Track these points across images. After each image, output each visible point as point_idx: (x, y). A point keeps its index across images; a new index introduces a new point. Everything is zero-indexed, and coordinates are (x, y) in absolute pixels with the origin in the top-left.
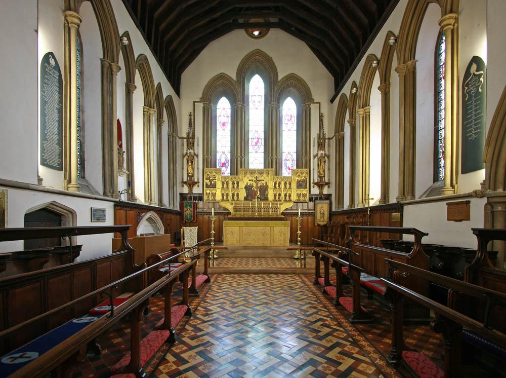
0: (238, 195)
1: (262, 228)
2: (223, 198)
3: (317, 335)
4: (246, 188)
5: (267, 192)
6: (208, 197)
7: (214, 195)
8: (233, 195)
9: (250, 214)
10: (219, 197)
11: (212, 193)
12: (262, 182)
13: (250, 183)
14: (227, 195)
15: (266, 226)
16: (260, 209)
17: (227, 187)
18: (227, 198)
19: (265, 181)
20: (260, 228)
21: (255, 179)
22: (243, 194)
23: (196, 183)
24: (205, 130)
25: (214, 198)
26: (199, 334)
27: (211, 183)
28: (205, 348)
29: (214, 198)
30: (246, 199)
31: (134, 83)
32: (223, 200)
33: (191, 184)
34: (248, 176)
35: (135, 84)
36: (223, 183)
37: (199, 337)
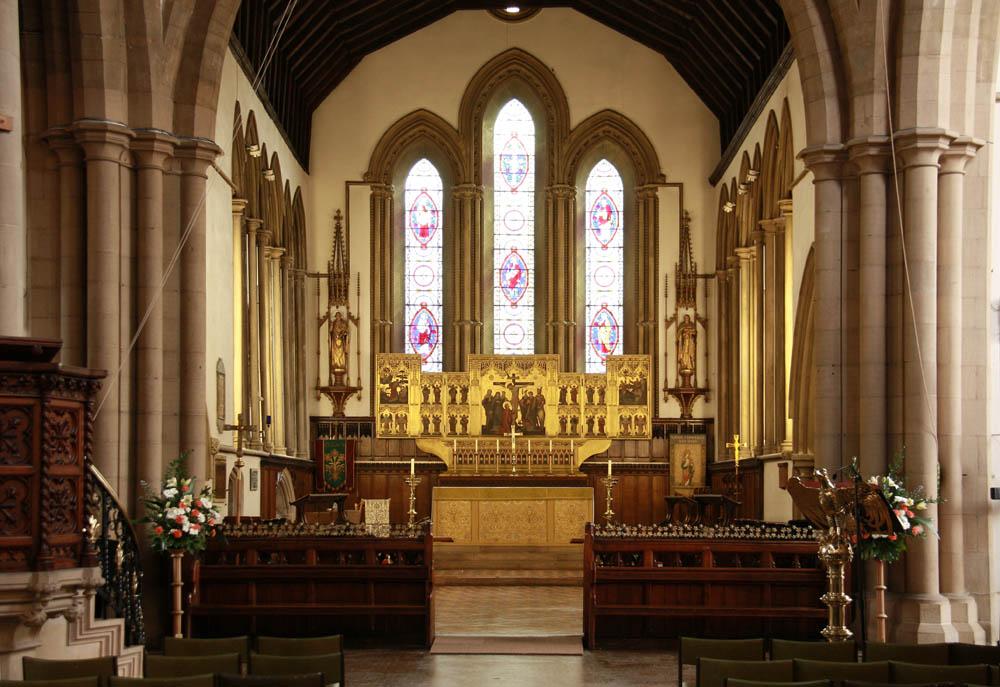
1: (527, 503)
2: (426, 428)
4: (486, 403)
5: (541, 414)
7: (403, 421)
9: (496, 469)
10: (414, 427)
11: (397, 417)
12: (529, 388)
13: (495, 390)
14: (437, 421)
16: (522, 456)
17: (438, 401)
20: (521, 503)
23: (354, 390)
30: (486, 431)
32: (425, 434)
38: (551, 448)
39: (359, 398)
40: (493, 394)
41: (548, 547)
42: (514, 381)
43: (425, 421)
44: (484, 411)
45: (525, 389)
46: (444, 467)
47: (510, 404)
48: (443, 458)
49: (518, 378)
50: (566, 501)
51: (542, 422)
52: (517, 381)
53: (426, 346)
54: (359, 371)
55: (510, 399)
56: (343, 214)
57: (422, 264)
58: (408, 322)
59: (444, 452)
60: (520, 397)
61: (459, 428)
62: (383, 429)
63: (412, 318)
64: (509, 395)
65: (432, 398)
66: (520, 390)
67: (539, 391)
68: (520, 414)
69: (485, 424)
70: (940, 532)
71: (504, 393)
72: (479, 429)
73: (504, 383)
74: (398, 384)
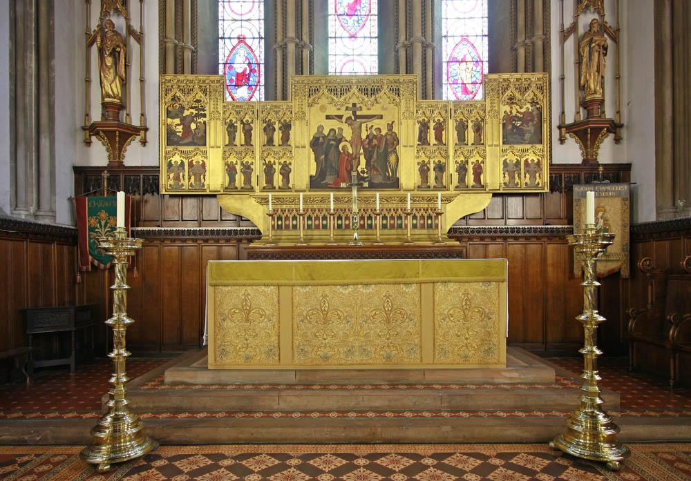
0: (286, 171)
1: (384, 290)
2: (232, 180)
5: (392, 158)
6: (177, 178)
7: (199, 171)
8: (269, 171)
9: (330, 236)
10: (215, 179)
11: (191, 165)
12: (376, 123)
13: (328, 126)
14: (247, 170)
18: (248, 180)
20: (372, 289)
21: (350, 113)
22: (304, 166)
23: (136, 131)
27: (187, 129)
30: (315, 183)
32: (231, 189)
34: (323, 101)
36: (231, 129)
40: (326, 132)
42: (354, 113)
43: (231, 170)
44: (313, 156)
45: (369, 125)
46: (257, 234)
47: (349, 145)
48: (256, 223)
51: (395, 171)
52: (358, 113)
55: (349, 138)
58: (221, 59)
59: (257, 213)
60: (364, 136)
61: (278, 180)
65: (240, 137)
66: (364, 126)
68: (363, 161)
69: (313, 173)
73: (340, 117)
74: (192, 118)
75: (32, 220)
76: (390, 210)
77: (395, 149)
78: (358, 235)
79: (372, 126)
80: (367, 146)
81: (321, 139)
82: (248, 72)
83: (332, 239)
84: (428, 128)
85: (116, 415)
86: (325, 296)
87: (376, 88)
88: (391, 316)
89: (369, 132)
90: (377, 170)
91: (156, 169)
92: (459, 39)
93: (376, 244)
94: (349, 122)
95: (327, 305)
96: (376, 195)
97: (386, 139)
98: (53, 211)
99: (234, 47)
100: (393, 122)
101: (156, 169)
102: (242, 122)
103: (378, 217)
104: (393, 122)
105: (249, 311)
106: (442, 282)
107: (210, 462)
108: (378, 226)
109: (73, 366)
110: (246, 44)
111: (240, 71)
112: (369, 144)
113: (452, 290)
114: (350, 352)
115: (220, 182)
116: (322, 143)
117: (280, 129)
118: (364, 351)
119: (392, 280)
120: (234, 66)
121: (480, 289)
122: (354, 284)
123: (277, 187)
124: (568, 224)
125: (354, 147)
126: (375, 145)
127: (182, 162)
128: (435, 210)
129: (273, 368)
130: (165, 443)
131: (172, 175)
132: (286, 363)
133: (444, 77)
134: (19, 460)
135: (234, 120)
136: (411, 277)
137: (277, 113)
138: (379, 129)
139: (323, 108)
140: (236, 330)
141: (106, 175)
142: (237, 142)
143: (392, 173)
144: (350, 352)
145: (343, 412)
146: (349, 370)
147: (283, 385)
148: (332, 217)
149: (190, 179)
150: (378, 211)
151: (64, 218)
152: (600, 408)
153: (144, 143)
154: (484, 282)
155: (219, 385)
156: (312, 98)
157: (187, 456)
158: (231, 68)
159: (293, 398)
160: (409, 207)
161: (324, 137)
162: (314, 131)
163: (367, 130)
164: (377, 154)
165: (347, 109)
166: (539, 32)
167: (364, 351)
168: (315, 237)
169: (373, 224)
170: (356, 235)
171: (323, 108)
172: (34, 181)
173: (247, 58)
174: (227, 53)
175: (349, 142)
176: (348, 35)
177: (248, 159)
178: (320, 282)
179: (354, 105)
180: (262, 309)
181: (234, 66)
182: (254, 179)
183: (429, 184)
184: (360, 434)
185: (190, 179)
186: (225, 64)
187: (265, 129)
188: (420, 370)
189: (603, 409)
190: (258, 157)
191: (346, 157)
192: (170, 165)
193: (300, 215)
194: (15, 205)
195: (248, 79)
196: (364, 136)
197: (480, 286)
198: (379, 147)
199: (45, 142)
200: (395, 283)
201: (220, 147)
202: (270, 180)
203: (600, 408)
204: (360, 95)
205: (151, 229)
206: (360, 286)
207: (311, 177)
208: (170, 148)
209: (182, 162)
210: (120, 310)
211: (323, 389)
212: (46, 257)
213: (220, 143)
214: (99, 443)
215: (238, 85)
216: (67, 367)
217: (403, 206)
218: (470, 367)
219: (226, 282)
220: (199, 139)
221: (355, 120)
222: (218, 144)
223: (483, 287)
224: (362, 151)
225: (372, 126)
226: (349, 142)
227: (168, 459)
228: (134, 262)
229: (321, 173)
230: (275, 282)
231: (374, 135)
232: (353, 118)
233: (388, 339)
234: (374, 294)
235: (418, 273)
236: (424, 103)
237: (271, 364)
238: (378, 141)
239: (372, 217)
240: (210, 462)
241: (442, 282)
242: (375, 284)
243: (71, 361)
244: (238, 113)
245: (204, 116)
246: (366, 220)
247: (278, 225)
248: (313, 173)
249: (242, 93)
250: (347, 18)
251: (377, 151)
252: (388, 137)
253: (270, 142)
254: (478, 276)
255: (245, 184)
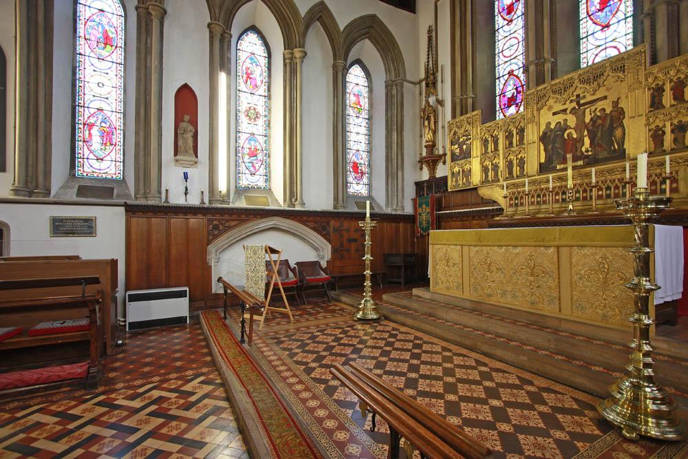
0: (522, 163)
1: (527, 251)
2: (487, 176)
3: (64, 426)
4: (544, 138)
5: (618, 133)
6: (457, 181)
7: (467, 174)
8: (510, 165)
9: (550, 208)
10: (476, 178)
11: (463, 171)
12: (600, 105)
13: (554, 121)
14: (496, 167)
15: (542, 244)
16: (584, 190)
17: (496, 149)
18: (496, 174)
19: (612, 97)
20: (518, 250)
21: (574, 104)
22: (535, 155)
23: (440, 157)
24: (32, 67)
25: (467, 180)
26: (71, 426)
27: (461, 149)
28: (124, 441)
29: (467, 180)
30: (543, 168)
31: (230, 31)
32: (485, 182)
33: (432, 160)
34: (551, 102)
35: (232, 32)
36: (485, 142)
37: (72, 431)
38: (594, 181)
39: (444, 163)
40: (552, 126)
41: (560, 320)
42: (578, 103)
43: (485, 170)
44: (542, 147)
45: (593, 108)
46: (502, 210)
47: (573, 131)
48: (501, 204)
49: (584, 97)
50: (593, 250)
51: (621, 143)
52: (582, 102)
53: (513, 107)
54: (444, 144)
55: (573, 125)
56: (434, 27)
57: (509, 38)
58: (498, 92)
59: (498, 194)
60: (587, 120)
61: (516, 170)
62: (454, 184)
63: (501, 88)
64: (572, 121)
65: (491, 147)
66: (587, 111)
67: (616, 104)
68: (587, 141)
69: (543, 160)
70: (367, 392)
71: (565, 120)
72: (536, 167)
73: (565, 111)
74: (464, 142)
75: (394, 213)
76: (614, 181)
77: (622, 122)
78: (573, 207)
79: (596, 109)
80: (591, 128)
81: (549, 133)
82: (515, 94)
83: (594, 208)
84: (664, 91)
85: (638, 382)
86: (488, 253)
87: (598, 74)
88: (533, 271)
89: (593, 115)
90: (601, 146)
91: (446, 177)
92: (507, 76)
93: (590, 213)
94: (573, 112)
95: (606, 266)
96: (665, 158)
97: (611, 117)
98: (403, 207)
99: (506, 81)
100: (619, 99)
101: (446, 177)
102: (492, 136)
103: (594, 189)
104: (619, 99)
105: (534, 268)
106: (578, 246)
107: (575, 406)
108: (594, 197)
109: (403, 283)
110: (514, 75)
111: (510, 96)
112: (593, 125)
113: (589, 253)
114: (504, 294)
115: (479, 179)
116: (550, 136)
117: (517, 134)
118: (514, 296)
119: (534, 243)
120: (506, 94)
121: (620, 254)
122: (506, 246)
123: (515, 176)
124: (371, 214)
125: (578, 132)
126: (600, 124)
127: (459, 170)
128: (623, 179)
129: (459, 296)
130: (387, 318)
131: (454, 179)
132: (466, 295)
133: (498, 106)
134: (425, 347)
135: (487, 136)
136: (549, 241)
137: (514, 123)
138: (604, 110)
139: (550, 108)
140: (593, 289)
141: (425, 185)
142: (489, 150)
143: (618, 145)
144: (504, 294)
145: (509, 340)
146: (502, 307)
147: (583, 336)
148: (551, 194)
149: (463, 180)
150: (527, 192)
151: (408, 209)
152: (649, 379)
153: (444, 163)
154: (624, 247)
155: (586, 337)
156: (540, 103)
157: (556, 392)
158: (504, 96)
159: (454, 315)
160: (628, 176)
161: (551, 130)
162: (543, 128)
163: (591, 114)
164: (602, 132)
165: (571, 101)
166: (458, 101)
167: (514, 296)
168: (542, 210)
169: (588, 196)
170: (571, 207)
171: (550, 108)
172: (396, 194)
173: (515, 85)
174: (501, 86)
175: (574, 129)
176: (600, 28)
177: (496, 161)
178: (484, 243)
179: (578, 96)
180: (622, 273)
181: (506, 94)
182: (499, 174)
183: (664, 148)
184: (468, 342)
185: (463, 180)
186: (500, 95)
187: (507, 137)
188: (557, 318)
189: (654, 380)
190: (501, 158)
191: (571, 142)
192: (453, 173)
193: (526, 195)
194: (387, 205)
195: (516, 99)
196: (587, 120)
197: (620, 251)
198: (603, 125)
199: (400, 174)
200: (535, 246)
201: (642, 115)
202: (511, 173)
203: (649, 379)
204: (614, 75)
205: (488, 208)
206: (510, 247)
207: (540, 164)
208: (452, 164)
209: (459, 170)
210: (368, 254)
211: (539, 329)
212: (398, 229)
213: (479, 154)
214: (359, 309)
215: (509, 106)
216: (400, 283)
217: (623, 176)
218: (609, 326)
219: (437, 242)
220: (467, 155)
221: (579, 108)
222: (641, 113)
223: (623, 252)
224: (586, 133)
225: (596, 109)
226: (574, 129)
227: (538, 388)
228: (373, 231)
229: (549, 159)
230: (460, 243)
231: (598, 116)
232: (577, 108)
233: (532, 289)
234: (521, 254)
235: (555, 238)
236: (655, 69)
237: (458, 294)
238: (602, 121)
239: (586, 190)
240: (575, 406)
241: (578, 246)
242: (522, 246)
243: (402, 280)
244: (489, 131)
245: (470, 139)
246: (658, 185)
247: (661, 189)
248: (543, 160)
249: (512, 110)
250: (600, 13)
251: (602, 129)
252: (613, 114)
253: (511, 144)
254: (617, 241)
255: (494, 177)
